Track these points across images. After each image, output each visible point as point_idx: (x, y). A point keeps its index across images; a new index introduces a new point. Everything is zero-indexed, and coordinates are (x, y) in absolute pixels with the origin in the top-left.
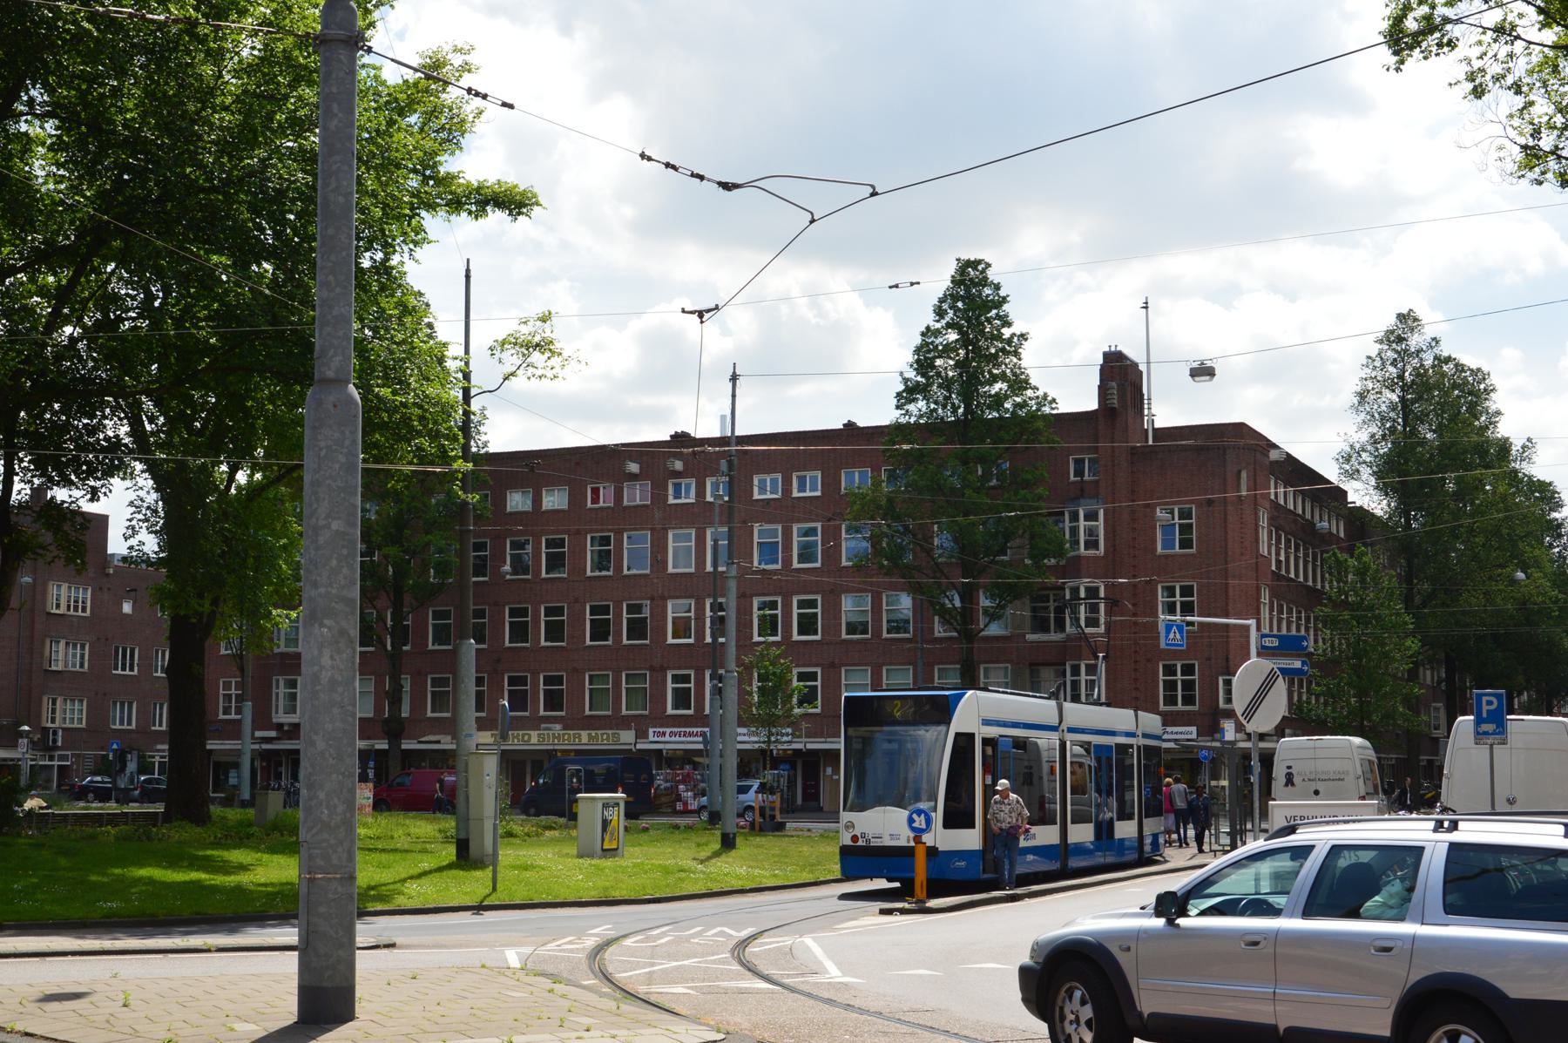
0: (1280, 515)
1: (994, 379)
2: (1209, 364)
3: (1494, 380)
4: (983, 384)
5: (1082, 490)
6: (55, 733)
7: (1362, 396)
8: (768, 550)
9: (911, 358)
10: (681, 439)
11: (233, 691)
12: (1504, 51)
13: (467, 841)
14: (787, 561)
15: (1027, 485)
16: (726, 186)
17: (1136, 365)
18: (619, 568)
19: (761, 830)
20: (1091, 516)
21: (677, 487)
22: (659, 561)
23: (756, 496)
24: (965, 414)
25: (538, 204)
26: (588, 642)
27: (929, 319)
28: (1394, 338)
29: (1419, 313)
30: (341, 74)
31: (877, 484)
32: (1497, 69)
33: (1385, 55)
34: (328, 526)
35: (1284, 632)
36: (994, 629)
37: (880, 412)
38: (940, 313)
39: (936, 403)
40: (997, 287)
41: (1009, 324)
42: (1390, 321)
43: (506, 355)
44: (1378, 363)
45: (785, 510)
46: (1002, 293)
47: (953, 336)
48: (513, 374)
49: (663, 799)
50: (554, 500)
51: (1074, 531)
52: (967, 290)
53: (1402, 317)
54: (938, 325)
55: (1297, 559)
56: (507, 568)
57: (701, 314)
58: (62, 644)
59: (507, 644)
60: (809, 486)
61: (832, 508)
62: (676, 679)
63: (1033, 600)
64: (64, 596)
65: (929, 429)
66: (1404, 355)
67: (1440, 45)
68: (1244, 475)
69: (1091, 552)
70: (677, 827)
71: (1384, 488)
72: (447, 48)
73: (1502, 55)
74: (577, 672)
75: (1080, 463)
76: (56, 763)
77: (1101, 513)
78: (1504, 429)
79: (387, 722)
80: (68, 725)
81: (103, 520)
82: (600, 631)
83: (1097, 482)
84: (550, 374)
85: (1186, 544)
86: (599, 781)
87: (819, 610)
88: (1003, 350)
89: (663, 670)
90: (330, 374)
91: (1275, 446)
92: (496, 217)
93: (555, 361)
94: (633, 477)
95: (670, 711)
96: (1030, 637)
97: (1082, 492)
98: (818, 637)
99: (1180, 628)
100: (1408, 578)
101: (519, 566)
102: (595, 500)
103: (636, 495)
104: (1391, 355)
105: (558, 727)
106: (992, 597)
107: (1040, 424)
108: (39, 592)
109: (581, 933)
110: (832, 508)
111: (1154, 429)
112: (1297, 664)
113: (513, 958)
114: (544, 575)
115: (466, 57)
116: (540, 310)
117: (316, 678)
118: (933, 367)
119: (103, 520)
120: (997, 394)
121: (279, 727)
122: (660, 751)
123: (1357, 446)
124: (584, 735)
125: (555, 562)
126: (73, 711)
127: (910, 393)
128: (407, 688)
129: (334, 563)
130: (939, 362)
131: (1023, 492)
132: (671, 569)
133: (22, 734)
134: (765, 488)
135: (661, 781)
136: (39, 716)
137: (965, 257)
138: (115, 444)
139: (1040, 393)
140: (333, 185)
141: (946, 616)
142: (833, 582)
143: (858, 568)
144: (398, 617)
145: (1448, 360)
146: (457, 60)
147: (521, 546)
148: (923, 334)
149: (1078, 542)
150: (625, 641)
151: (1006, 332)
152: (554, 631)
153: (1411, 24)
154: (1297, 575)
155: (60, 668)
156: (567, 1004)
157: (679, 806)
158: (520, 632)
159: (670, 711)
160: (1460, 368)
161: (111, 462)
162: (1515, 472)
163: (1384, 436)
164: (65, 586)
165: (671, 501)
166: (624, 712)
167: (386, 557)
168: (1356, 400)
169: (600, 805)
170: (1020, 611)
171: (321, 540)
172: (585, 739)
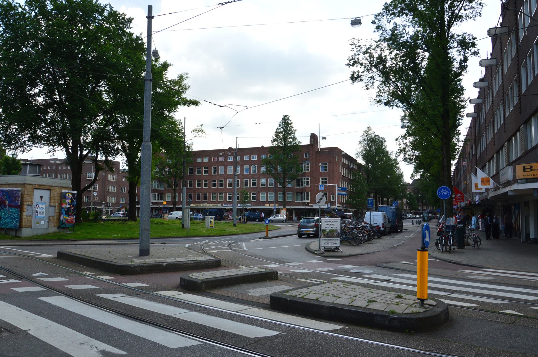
0: (344, 165)
1: (290, 138)
2: (325, 137)
3: (386, 140)
4: (288, 139)
5: (306, 159)
6: (109, 204)
7: (360, 142)
8: (247, 170)
9: (274, 134)
10: (230, 149)
11: (324, 180)
12: (372, 81)
13: (184, 225)
14: (250, 172)
15: (295, 158)
16: (220, 106)
17: (317, 136)
18: (218, 173)
19: (242, 223)
20: (308, 164)
21: (229, 158)
22: (226, 172)
23: (244, 160)
24: (284, 145)
25: (200, 104)
26: (212, 187)
27: (278, 126)
28: (366, 131)
29: (371, 127)
30: (149, 86)
31: (267, 157)
32: (371, 85)
33: (351, 81)
34: (145, 168)
35: (343, 187)
36: (290, 186)
37: (268, 143)
38: (280, 125)
39: (279, 142)
40: (291, 121)
41: (293, 128)
42: (365, 128)
43: (194, 133)
44: (363, 136)
45: (250, 163)
46: (292, 122)
47: (282, 130)
48: (196, 136)
49: (226, 217)
50: (206, 160)
51: (305, 167)
52: (285, 121)
53: (368, 128)
54: (279, 128)
55: (347, 173)
56: (196, 173)
57: (221, 128)
58: (111, 186)
59: (196, 187)
60: (255, 158)
61: (259, 163)
62: (229, 194)
63: (297, 180)
64: (111, 177)
65: (278, 147)
66: (368, 135)
67: (360, 80)
68: (337, 157)
69: (308, 171)
70: (227, 223)
71: (364, 159)
72: (184, 73)
73: (372, 82)
74: (210, 193)
75: (306, 154)
76: (110, 209)
77: (310, 164)
78: (387, 149)
79: (173, 202)
80: (112, 202)
81: (119, 163)
82: (214, 185)
83: (309, 158)
84: (203, 136)
85: (326, 170)
86: (213, 213)
87: (256, 182)
88: (292, 133)
89: (226, 193)
90: (146, 140)
91: (343, 152)
92: (192, 106)
93: (204, 134)
94: (221, 156)
95: (228, 201)
96: (296, 187)
97: (306, 160)
98: (256, 187)
99: (323, 186)
100: (368, 177)
101: (199, 172)
102: (214, 160)
103: (221, 159)
104: (366, 135)
105: (206, 203)
106: (289, 180)
107: (298, 147)
108: (106, 177)
109: (201, 241)
110: (259, 163)
111: (320, 148)
112: (345, 193)
113: (187, 246)
114: (204, 174)
115: (187, 75)
116: (201, 124)
117: (143, 195)
118: (278, 135)
119: (119, 163)
120: (290, 141)
121: (152, 203)
122: (225, 208)
123: (359, 152)
124: (211, 205)
125: (206, 172)
126: (113, 199)
127: (274, 140)
128: (177, 195)
129: (146, 174)
130: (279, 135)
131: (295, 160)
132: (228, 174)
133: (103, 204)
134: (246, 158)
135: (225, 214)
136: (106, 200)
137: (285, 115)
138: (118, 149)
139: (299, 141)
140: (147, 106)
141: (280, 184)
142: (259, 176)
143: (263, 173)
144: (175, 182)
145: (377, 136)
146: (185, 76)
147: (200, 168)
148: (277, 129)
149: (305, 169)
150: (219, 187)
151: (292, 129)
152: (206, 185)
153: (355, 76)
154: (349, 177)
155: (110, 191)
156: (188, 253)
157: (229, 219)
158: (199, 185)
159: (228, 201)
160: (379, 137)
161: (117, 152)
162: (389, 157)
163: (364, 150)
164: (111, 175)
165: (228, 160)
166: (219, 201)
167: (173, 170)
168: (359, 143)
169: (210, 218)
170: (294, 182)
171: (144, 170)
172: (211, 206)
